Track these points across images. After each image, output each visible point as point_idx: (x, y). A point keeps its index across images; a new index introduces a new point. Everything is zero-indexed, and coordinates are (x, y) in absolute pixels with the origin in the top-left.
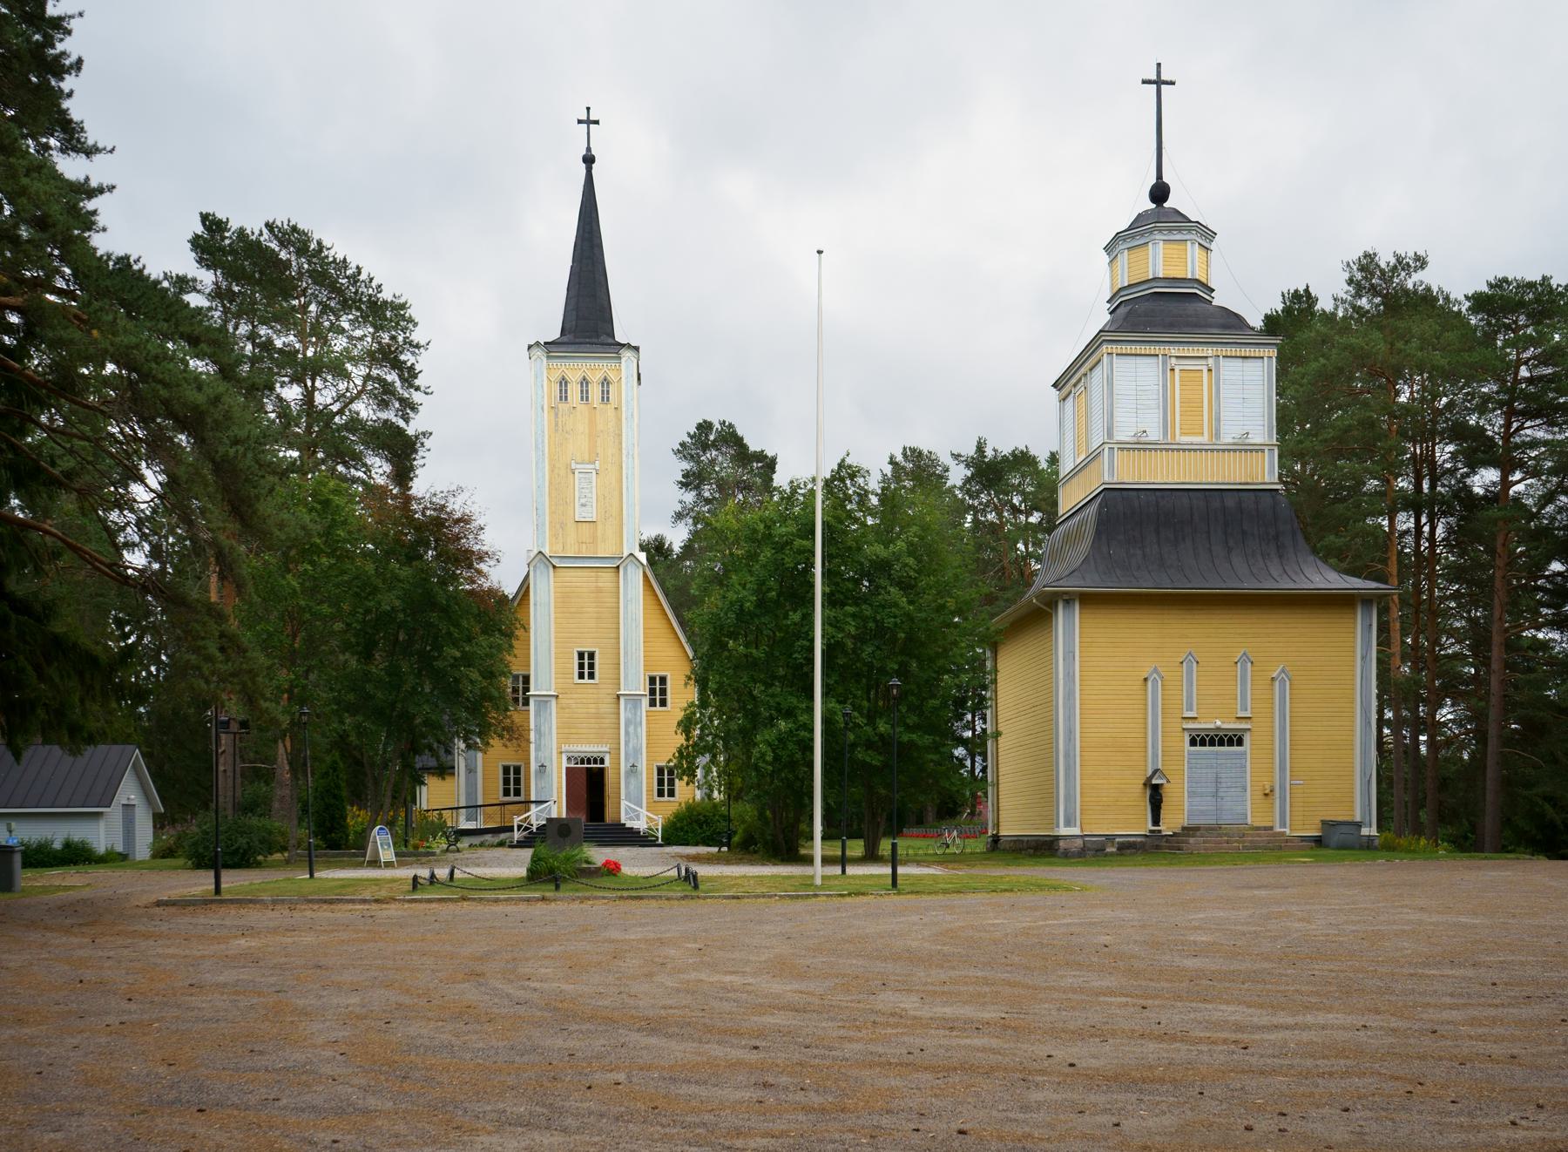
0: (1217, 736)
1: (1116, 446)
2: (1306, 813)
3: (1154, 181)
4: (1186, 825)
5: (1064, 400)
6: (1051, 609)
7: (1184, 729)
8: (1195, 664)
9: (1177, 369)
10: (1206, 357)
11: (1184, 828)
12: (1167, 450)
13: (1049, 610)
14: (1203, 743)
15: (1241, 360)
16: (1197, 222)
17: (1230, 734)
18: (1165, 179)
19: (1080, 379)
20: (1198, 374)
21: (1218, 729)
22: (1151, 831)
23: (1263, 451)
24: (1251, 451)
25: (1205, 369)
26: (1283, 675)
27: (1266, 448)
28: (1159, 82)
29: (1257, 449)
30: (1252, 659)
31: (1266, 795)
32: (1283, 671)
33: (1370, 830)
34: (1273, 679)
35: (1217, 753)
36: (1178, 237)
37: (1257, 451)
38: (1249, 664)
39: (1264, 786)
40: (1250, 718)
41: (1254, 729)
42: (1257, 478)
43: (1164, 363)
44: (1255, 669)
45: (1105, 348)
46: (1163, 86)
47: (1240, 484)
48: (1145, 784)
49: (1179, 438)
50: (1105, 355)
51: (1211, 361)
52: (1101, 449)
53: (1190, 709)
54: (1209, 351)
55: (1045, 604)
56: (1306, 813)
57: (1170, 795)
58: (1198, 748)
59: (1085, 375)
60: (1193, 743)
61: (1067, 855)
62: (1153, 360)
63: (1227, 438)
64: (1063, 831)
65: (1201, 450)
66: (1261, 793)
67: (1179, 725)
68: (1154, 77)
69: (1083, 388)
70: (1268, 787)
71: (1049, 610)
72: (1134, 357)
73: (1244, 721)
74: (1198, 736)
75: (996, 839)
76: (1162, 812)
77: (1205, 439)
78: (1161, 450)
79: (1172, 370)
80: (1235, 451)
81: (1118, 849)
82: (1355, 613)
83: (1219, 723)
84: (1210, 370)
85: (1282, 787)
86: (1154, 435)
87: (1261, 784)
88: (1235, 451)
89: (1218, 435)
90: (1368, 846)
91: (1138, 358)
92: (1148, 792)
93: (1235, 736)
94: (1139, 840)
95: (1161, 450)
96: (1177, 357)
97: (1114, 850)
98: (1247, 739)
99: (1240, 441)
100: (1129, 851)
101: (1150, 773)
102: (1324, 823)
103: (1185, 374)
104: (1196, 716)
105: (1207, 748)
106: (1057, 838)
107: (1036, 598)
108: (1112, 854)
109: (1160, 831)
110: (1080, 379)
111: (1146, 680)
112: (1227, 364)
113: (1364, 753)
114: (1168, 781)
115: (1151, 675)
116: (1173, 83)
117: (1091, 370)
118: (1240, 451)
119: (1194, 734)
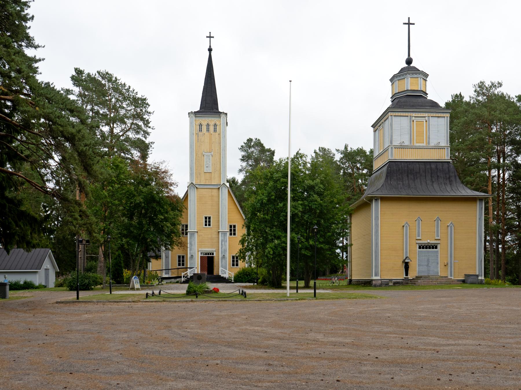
0: (428, 245)
1: (393, 147)
3: (407, 57)
4: (417, 276)
7: (417, 243)
8: (420, 221)
9: (415, 121)
10: (425, 117)
15: (437, 118)
19: (381, 124)
20: (422, 123)
21: (429, 243)
22: (405, 278)
23: (445, 149)
25: (425, 121)
27: (446, 148)
28: (409, 24)
29: (443, 148)
30: (441, 219)
31: (445, 265)
32: (451, 223)
34: (448, 226)
35: (428, 251)
36: (416, 76)
37: (443, 148)
38: (440, 221)
39: (444, 262)
40: (440, 239)
41: (441, 243)
43: (410, 119)
44: (442, 222)
45: (390, 114)
46: (411, 25)
48: (403, 262)
50: (390, 116)
52: (388, 148)
53: (419, 236)
58: (421, 250)
59: (383, 123)
60: (420, 248)
63: (432, 144)
64: (374, 278)
65: (423, 148)
66: (444, 265)
69: (382, 127)
70: (446, 263)
72: (400, 117)
73: (437, 240)
77: (424, 144)
78: (409, 148)
79: (413, 121)
82: (477, 204)
83: (429, 241)
84: (426, 121)
86: (407, 143)
87: (444, 262)
89: (429, 143)
90: (481, 283)
91: (401, 117)
94: (401, 281)
96: (415, 117)
97: (392, 284)
98: (439, 246)
99: (437, 145)
101: (405, 258)
103: (417, 123)
107: (365, 198)
108: (391, 286)
109: (408, 278)
110: (381, 124)
111: (403, 226)
114: (411, 261)
116: (414, 24)
117: (385, 121)
119: (420, 245)
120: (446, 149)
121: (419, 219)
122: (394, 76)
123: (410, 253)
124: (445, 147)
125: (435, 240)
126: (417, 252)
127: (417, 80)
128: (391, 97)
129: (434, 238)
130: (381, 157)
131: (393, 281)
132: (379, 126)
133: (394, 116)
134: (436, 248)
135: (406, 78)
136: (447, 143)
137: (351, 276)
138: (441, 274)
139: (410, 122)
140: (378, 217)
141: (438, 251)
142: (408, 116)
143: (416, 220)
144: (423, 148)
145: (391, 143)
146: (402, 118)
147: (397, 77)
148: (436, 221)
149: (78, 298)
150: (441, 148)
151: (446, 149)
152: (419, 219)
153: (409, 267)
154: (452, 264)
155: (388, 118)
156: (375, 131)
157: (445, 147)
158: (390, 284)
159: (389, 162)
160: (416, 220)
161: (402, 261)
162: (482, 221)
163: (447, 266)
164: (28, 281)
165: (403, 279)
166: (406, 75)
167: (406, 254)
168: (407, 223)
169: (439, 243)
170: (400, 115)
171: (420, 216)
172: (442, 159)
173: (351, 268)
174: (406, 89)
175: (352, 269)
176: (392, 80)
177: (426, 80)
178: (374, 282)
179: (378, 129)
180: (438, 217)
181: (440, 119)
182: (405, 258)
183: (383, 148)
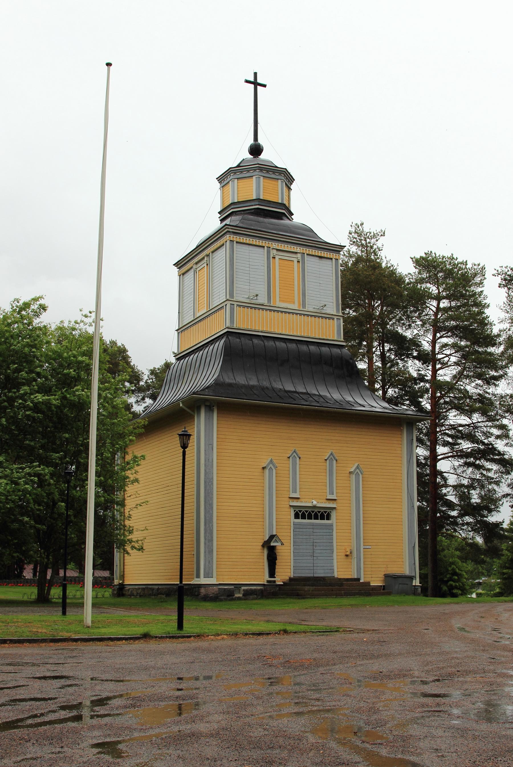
0: (313, 512)
1: (236, 303)
2: (373, 569)
3: (251, 141)
4: (292, 576)
5: (183, 274)
6: (193, 411)
7: (290, 506)
8: (298, 459)
9: (277, 258)
10: (296, 253)
11: (291, 579)
12: (270, 310)
13: (192, 413)
14: (303, 517)
15: (318, 258)
16: (286, 169)
17: (322, 511)
18: (260, 141)
19: (203, 258)
20: (291, 263)
21: (315, 507)
22: (268, 581)
23: (333, 319)
24: (326, 318)
25: (295, 260)
26: (358, 470)
27: (335, 318)
28: (256, 84)
29: (330, 317)
30: (337, 458)
31: (347, 556)
32: (358, 467)
33: (417, 582)
34: (350, 473)
35: (313, 525)
36: (273, 176)
37: (329, 318)
38: (335, 461)
39: (345, 549)
40: (335, 500)
41: (338, 508)
42: (330, 336)
43: (268, 253)
44: (339, 465)
45: (227, 237)
46: (258, 87)
47: (320, 339)
48: (263, 546)
49: (279, 304)
50: (228, 242)
51: (299, 256)
52: (224, 304)
53: (295, 491)
54: (298, 249)
55: (189, 408)
56: (373, 569)
57: (281, 554)
58: (300, 521)
59: (208, 255)
60: (297, 516)
61: (206, 598)
62: (261, 250)
63: (310, 308)
64: (203, 581)
65: (293, 313)
66: (344, 554)
67: (287, 503)
68: (252, 79)
69: (205, 265)
70: (348, 550)
71: (192, 413)
72: (248, 246)
73: (331, 502)
74: (300, 511)
75: (122, 587)
76: (277, 567)
77: (295, 306)
78: (267, 310)
79: (274, 258)
80: (315, 316)
81: (243, 595)
82: (402, 431)
83: (315, 503)
84: (298, 262)
85: (358, 550)
86: (263, 299)
87: (343, 548)
88: (315, 316)
89: (304, 306)
90: (414, 592)
91: (250, 247)
92: (266, 552)
93: (325, 512)
94: (259, 588)
95: (267, 310)
96: (277, 250)
97: (241, 595)
98: (333, 515)
99: (318, 311)
100: (251, 597)
101: (267, 538)
102: (387, 576)
103: (282, 261)
104: (299, 496)
105: (306, 521)
106: (200, 586)
107: (183, 403)
108: (239, 599)
109: (275, 581)
110: (203, 258)
111: (264, 468)
112: (309, 259)
113: (410, 528)
114: (282, 544)
115: (268, 465)
116: (264, 86)
117: (213, 252)
118: (319, 317)
119: (297, 510)
120: (335, 319)
121: (295, 454)
122: (230, 171)
123: (279, 527)
124: (333, 317)
125: (327, 502)
126: (292, 525)
127: (276, 183)
128: (220, 210)
129: (325, 498)
130: (200, 324)
131: (243, 588)
132: (196, 263)
133: (237, 242)
134: (328, 518)
135: (254, 177)
136: (338, 310)
137: (124, 577)
138: (339, 573)
139: (268, 258)
140: (212, 445)
141: (332, 525)
142: (264, 247)
143: (289, 458)
144: (293, 313)
145: (232, 294)
146: (251, 248)
147: (235, 173)
148: (328, 461)
149: (180, 626)
150: (326, 318)
151: (335, 319)
152: (295, 456)
153: (278, 557)
154: (360, 552)
155: (223, 245)
156: (182, 275)
157: (333, 317)
158: (237, 595)
159: (228, 332)
160: (289, 458)
161: (261, 544)
162: (413, 466)
163: (350, 557)
164: (139, 368)
165: (264, 585)
166: (255, 170)
167: (269, 531)
168: (271, 461)
169: (335, 508)
170: (248, 242)
171: (297, 449)
172: (328, 338)
173: (124, 560)
174: (254, 198)
175: (125, 561)
176: (222, 179)
177: (289, 189)
178: (203, 591)
179: (192, 268)
180: (332, 454)
181: (324, 261)
182: (267, 538)
183: (209, 304)
